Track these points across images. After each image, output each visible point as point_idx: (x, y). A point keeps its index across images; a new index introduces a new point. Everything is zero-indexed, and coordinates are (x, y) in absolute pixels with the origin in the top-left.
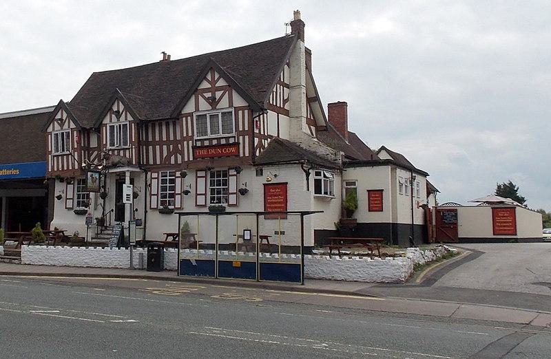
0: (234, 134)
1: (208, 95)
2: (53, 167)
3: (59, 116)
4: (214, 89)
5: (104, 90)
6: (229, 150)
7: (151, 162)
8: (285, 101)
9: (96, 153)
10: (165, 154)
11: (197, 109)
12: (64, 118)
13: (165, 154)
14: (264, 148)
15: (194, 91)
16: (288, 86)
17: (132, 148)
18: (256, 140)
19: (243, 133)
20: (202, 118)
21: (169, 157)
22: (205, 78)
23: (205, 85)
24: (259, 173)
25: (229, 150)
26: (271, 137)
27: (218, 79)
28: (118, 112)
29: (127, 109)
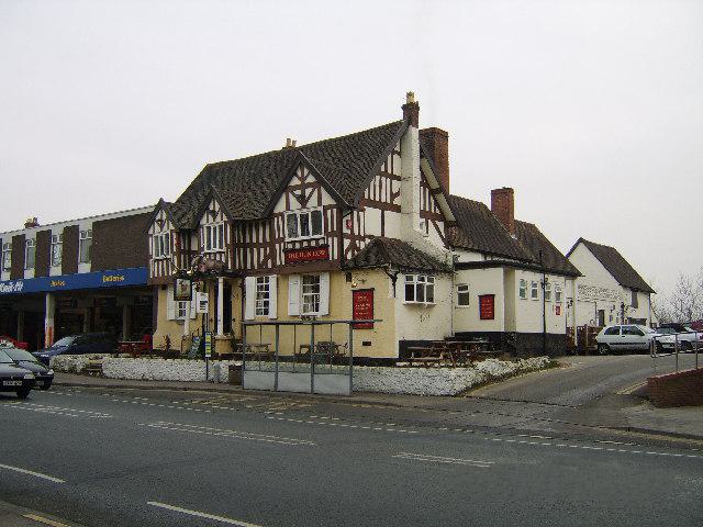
1: (298, 192)
3: (158, 217)
4: (303, 187)
5: (215, 181)
7: (249, 267)
8: (393, 196)
11: (288, 208)
12: (217, 209)
13: (262, 258)
14: (358, 249)
15: (284, 188)
16: (399, 179)
18: (347, 243)
19: (332, 234)
20: (293, 217)
21: (265, 262)
22: (295, 174)
23: (295, 182)
24: (349, 279)
26: (370, 237)
29: (223, 210)
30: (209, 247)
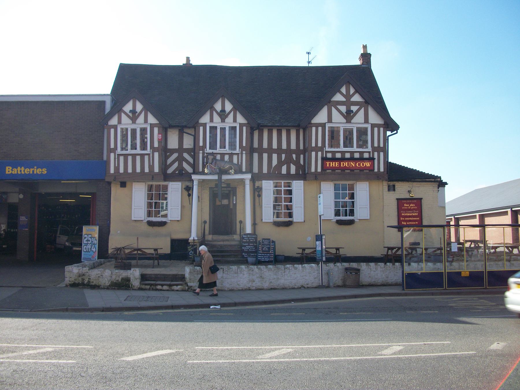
0: (370, 149)
2: (117, 168)
5: (134, 80)
6: (363, 164)
9: (175, 155)
10: (275, 162)
11: (330, 120)
13: (275, 162)
17: (242, 154)
23: (338, 97)
25: (363, 164)
27: (354, 94)
28: (223, 111)
30: (213, 146)
